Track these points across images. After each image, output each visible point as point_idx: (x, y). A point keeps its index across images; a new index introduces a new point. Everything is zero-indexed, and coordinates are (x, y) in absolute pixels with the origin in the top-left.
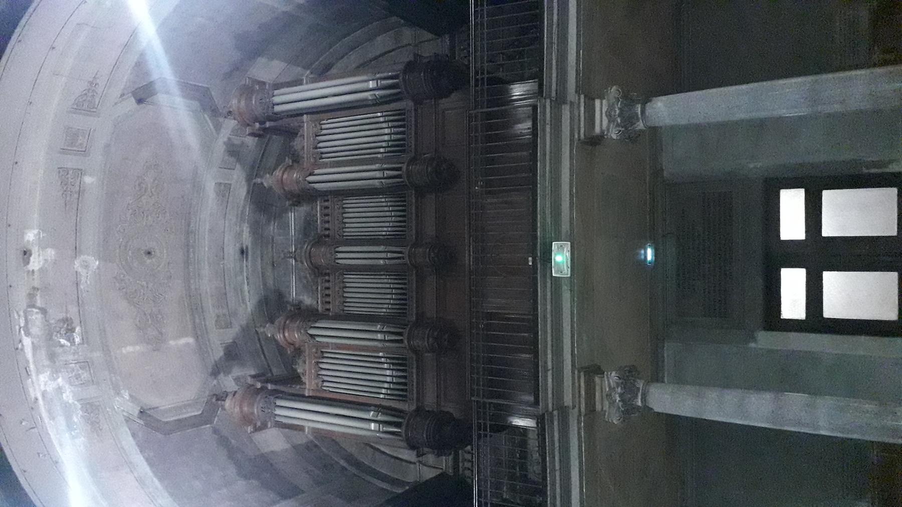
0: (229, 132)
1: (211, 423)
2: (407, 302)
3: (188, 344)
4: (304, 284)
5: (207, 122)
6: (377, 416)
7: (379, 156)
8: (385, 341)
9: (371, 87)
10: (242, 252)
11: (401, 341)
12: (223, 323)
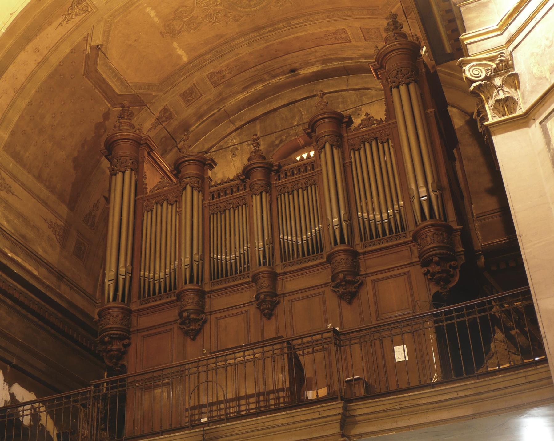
3: (179, 57)
4: (274, 142)
6: (267, 244)
8: (292, 242)
10: (293, 71)
11: (336, 243)
12: (215, 78)
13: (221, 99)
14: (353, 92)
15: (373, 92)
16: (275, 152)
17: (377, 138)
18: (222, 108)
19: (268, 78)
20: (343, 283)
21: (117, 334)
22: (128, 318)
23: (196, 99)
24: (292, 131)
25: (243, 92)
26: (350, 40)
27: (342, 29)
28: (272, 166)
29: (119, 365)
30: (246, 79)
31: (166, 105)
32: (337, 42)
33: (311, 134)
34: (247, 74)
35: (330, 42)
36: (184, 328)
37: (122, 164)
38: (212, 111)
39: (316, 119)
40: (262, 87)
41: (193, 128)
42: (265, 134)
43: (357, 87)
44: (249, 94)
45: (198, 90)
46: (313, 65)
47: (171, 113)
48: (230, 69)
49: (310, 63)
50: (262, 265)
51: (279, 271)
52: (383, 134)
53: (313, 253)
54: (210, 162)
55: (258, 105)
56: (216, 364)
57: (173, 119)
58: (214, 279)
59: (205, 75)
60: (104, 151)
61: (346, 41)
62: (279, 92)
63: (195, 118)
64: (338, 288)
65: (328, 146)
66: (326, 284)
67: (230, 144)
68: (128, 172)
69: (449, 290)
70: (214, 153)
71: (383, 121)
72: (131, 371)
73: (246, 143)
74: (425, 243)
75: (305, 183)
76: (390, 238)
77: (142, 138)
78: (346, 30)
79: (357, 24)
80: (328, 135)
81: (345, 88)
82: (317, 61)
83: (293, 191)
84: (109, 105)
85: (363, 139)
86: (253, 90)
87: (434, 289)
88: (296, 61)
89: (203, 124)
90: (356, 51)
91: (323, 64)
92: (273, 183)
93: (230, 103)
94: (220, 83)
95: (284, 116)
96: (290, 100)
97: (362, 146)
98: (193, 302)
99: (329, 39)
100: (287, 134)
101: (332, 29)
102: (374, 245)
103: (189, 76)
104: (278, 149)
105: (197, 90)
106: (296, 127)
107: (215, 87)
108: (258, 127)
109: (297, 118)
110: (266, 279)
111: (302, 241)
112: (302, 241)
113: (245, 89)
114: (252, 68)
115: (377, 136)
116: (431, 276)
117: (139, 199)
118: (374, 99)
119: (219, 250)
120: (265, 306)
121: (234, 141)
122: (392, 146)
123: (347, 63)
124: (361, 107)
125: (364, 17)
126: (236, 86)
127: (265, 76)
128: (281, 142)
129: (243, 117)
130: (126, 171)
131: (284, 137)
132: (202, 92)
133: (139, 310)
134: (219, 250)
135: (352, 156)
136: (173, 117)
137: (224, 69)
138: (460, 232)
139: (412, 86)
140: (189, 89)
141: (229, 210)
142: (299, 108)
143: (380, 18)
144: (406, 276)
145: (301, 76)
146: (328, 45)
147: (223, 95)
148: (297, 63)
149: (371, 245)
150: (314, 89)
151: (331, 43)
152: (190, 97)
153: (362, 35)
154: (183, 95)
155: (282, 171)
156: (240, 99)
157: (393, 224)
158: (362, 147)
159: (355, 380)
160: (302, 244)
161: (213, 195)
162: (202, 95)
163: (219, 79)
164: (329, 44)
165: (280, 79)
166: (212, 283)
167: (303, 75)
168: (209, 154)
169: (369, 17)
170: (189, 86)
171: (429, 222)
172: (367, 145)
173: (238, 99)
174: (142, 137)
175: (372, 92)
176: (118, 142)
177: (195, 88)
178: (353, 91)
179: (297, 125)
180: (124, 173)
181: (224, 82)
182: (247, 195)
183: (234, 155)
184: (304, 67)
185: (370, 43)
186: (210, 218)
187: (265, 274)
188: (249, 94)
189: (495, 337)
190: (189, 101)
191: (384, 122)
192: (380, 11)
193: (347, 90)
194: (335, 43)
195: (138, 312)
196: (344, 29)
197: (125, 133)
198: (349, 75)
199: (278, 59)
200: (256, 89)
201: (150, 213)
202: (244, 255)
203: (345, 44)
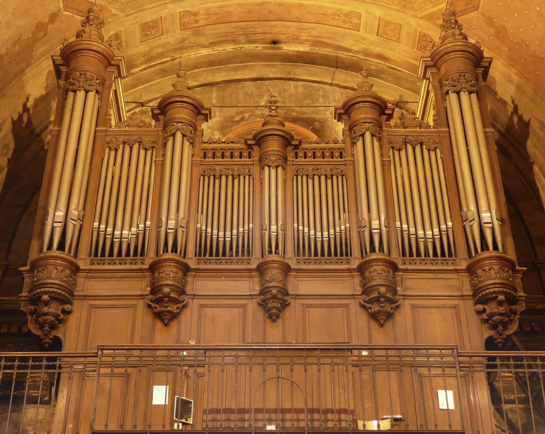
0: (424, 31)
1: (66, 8)
2: (221, 257)
4: (233, 117)
5: (434, 6)
7: (398, 224)
9: (442, 226)
10: (274, 42)
11: (373, 250)
12: (186, 20)
13: (181, 47)
14: (337, 89)
16: (233, 128)
17: (423, 142)
18: (176, 58)
19: (243, 41)
20: (381, 299)
21: (60, 294)
22: (74, 276)
23: (155, 36)
24: (257, 111)
25: (208, 47)
26: (359, 28)
27: (357, 13)
28: (293, 138)
29: (52, 337)
30: (220, 33)
31: (121, 31)
32: (344, 26)
33: (342, 116)
34: (222, 28)
35: (335, 23)
36: (156, 308)
37: (87, 81)
38: (165, 57)
39: (354, 102)
40: (233, 49)
42: (222, 105)
43: (344, 84)
44: (214, 52)
45: (162, 26)
46: (301, 43)
47: (121, 42)
48: (208, 15)
49: (300, 40)
50: (274, 253)
52: (431, 141)
53: (336, 255)
54: (207, 112)
55: (219, 69)
56: (127, 359)
57: (119, 50)
58: (200, 255)
59: (178, 10)
61: (354, 28)
62: (247, 62)
63: (142, 59)
64: (371, 303)
65: (368, 135)
66: (353, 296)
68: (93, 93)
69: (505, 337)
71: (430, 126)
72: (69, 347)
74: (488, 276)
75: (331, 170)
76: (341, 260)
77: (115, 58)
78: (361, 15)
79: (378, 12)
80: (369, 123)
81: (329, 81)
82: (307, 40)
84: (62, 6)
85: (405, 139)
86: (220, 49)
87: (488, 333)
88: (285, 33)
89: (149, 70)
90: (358, 43)
91: (313, 45)
92: (289, 159)
93: (189, 55)
94: (190, 27)
95: (250, 91)
96: (261, 75)
97: (404, 146)
98: (176, 277)
99: (336, 20)
100: (251, 113)
101: (346, 9)
102: (415, 264)
103: (161, 5)
104: (237, 126)
105: (161, 26)
106: (264, 108)
107: (182, 30)
110: (277, 271)
111: (225, 237)
112: (225, 237)
113: (212, 44)
114: (233, 22)
115: (423, 141)
116: (488, 317)
117: (102, 131)
120: (275, 304)
123: (342, 54)
125: (392, 7)
126: (204, 37)
127: (242, 38)
128: (242, 119)
129: (197, 77)
130: (90, 91)
131: (247, 115)
132: (164, 30)
133: (90, 271)
136: (120, 49)
137: (201, 12)
138: (522, 274)
139: (474, 96)
140: (153, 21)
141: (227, 177)
142: (269, 87)
143: (411, 14)
144: (454, 309)
145: (283, 51)
146: (331, 25)
147: (186, 43)
148: (284, 34)
149: (410, 263)
150: (292, 72)
151: (335, 25)
152: (150, 31)
153: (377, 27)
154: (144, 26)
155: (301, 149)
156: (202, 54)
158: (403, 148)
162: (163, 34)
163: (191, 22)
164: (333, 25)
165: (256, 47)
166: (198, 259)
167: (286, 51)
168: (145, 108)
169: (397, 8)
170: (154, 17)
171: (491, 252)
172: (410, 148)
173: (200, 53)
174: (115, 56)
176: (76, 53)
177: (160, 24)
178: (338, 88)
181: (195, 27)
182: (253, 164)
184: (289, 42)
185: (381, 39)
186: (200, 179)
187: (276, 265)
188: (214, 52)
190: (146, 35)
192: (416, 5)
193: (331, 84)
194: (340, 26)
195: (88, 273)
196: (360, 13)
198: (336, 68)
199: (266, 23)
200: (225, 50)
201: (113, 153)
202: (243, 236)
203: (351, 30)
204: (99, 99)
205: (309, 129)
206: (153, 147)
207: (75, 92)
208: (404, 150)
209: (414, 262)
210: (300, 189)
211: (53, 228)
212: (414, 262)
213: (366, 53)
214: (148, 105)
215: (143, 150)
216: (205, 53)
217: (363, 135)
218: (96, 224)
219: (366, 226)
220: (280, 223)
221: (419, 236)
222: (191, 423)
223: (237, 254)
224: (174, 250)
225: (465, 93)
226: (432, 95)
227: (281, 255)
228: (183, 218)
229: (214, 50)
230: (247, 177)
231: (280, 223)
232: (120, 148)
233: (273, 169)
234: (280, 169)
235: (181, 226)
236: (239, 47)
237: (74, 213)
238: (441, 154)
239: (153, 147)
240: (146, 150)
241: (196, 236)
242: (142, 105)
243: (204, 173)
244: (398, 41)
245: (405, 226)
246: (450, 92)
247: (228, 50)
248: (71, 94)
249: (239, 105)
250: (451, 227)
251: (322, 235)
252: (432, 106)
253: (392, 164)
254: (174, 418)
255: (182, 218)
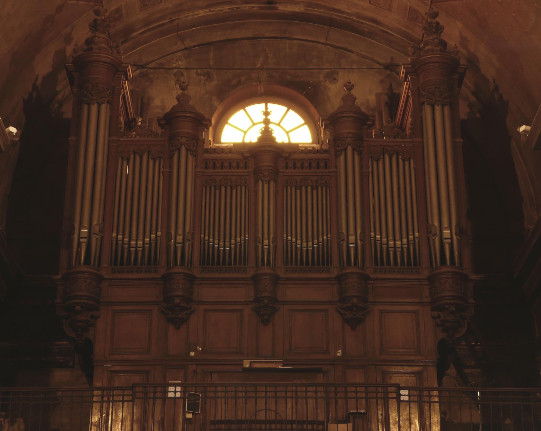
7: (372, 234)
15: (354, 57)
40: (229, 9)
41: (135, 34)
43: (338, 45)
44: (211, 13)
51: (282, 275)
60: (70, 65)
65: (349, 149)
67: (174, 65)
70: (151, 71)
73: (195, 71)
77: (123, 65)
81: (323, 41)
83: (301, 187)
93: (187, 17)
106: (259, 70)
108: (212, 54)
109: (261, 59)
112: (307, 247)
113: (209, 6)
118: (355, 66)
119: (211, 232)
121: (180, 63)
122: (413, 167)
124: (337, 70)
131: (243, 79)
134: (211, 232)
135: (370, 165)
139: (446, 109)
149: (381, 271)
157: (405, 255)
158: (381, 158)
159: (361, 413)
160: (307, 251)
161: (206, 163)
165: (253, 7)
168: (145, 69)
173: (197, 14)
175: (353, 55)
179: (261, 69)
180: (99, 105)
182: (249, 175)
183: (178, 82)
185: (374, 7)
186: (202, 190)
188: (211, 13)
189: (448, 372)
191: (408, 137)
193: (325, 44)
197: (105, 55)
200: (221, 10)
204: (110, 108)
205: (302, 95)
206: (160, 157)
207: (89, 104)
208: (382, 160)
209: (384, 271)
210: (289, 207)
211: (79, 244)
212: (384, 271)
213: (359, 16)
214: (147, 66)
215: (152, 160)
216: (202, 15)
217: (345, 150)
218: (114, 234)
219: (344, 240)
220: (271, 236)
221: (390, 246)
222: (200, 413)
223: (235, 264)
224: (182, 263)
225: (438, 106)
226: (411, 100)
227: (272, 267)
228: (189, 232)
229: (211, 10)
230: (243, 187)
231: (271, 236)
232: (131, 158)
233: (266, 184)
234: (272, 183)
235: (187, 240)
236: (236, 8)
237: (96, 229)
238: (414, 165)
239: (160, 157)
240: (154, 161)
241: (200, 253)
242: (142, 67)
243: (206, 184)
244: (390, 10)
245: (378, 237)
246: (426, 103)
247: (224, 11)
248: (86, 107)
249: (236, 67)
250: (418, 237)
251: (307, 244)
252: (410, 114)
253: (370, 175)
254: (186, 410)
255: (188, 232)
